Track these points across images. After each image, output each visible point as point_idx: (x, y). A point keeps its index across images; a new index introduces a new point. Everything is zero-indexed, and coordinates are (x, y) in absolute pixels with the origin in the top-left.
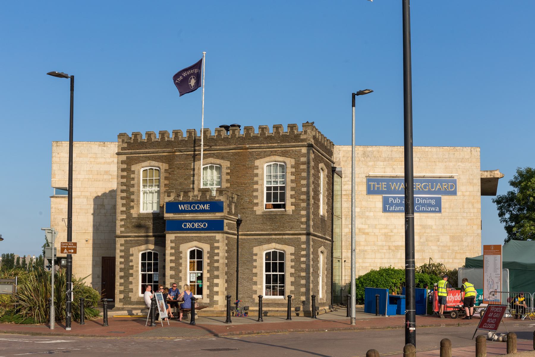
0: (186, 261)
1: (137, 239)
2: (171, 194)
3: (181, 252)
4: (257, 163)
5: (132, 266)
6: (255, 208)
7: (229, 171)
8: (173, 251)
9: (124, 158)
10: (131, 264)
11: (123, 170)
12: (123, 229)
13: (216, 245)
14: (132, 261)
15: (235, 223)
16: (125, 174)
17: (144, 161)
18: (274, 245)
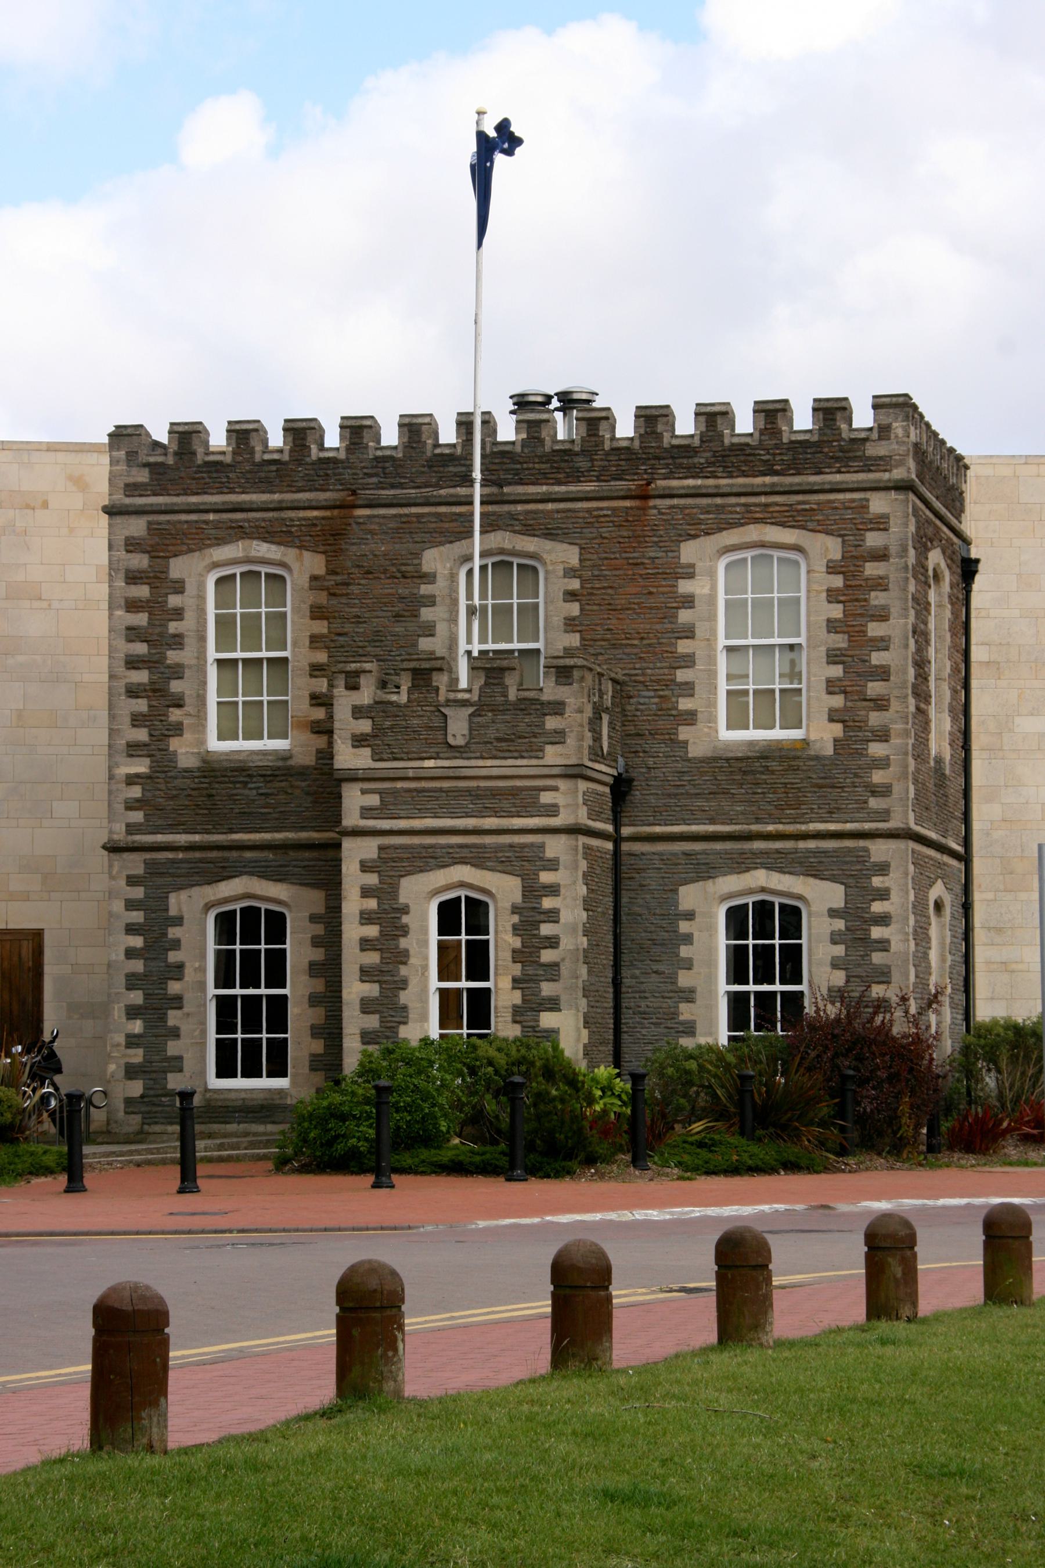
0: (425, 943)
1: (198, 855)
2: (363, 680)
3: (405, 910)
4: (689, 551)
5: (180, 967)
6: (684, 733)
7: (575, 584)
8: (372, 904)
9: (137, 527)
10: (173, 957)
11: (133, 578)
12: (138, 816)
13: (546, 877)
14: (176, 944)
15: (607, 790)
16: (143, 591)
17: (220, 541)
18: (760, 877)
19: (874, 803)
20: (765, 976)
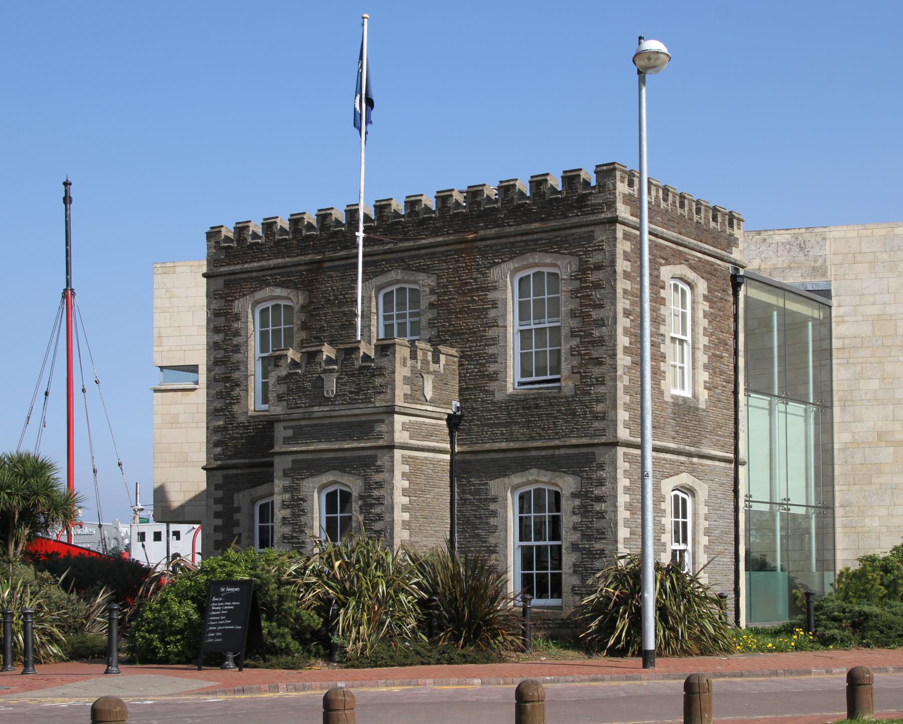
6: (492, 386)
15: (445, 423)
19: (596, 424)
20: (539, 536)
